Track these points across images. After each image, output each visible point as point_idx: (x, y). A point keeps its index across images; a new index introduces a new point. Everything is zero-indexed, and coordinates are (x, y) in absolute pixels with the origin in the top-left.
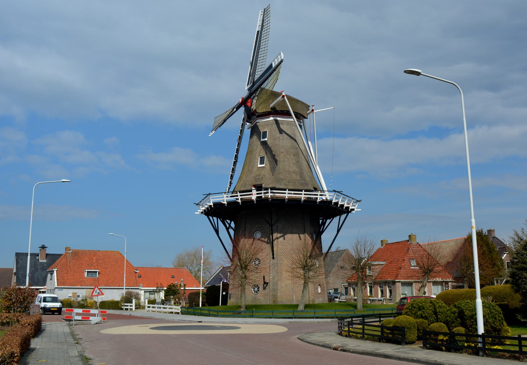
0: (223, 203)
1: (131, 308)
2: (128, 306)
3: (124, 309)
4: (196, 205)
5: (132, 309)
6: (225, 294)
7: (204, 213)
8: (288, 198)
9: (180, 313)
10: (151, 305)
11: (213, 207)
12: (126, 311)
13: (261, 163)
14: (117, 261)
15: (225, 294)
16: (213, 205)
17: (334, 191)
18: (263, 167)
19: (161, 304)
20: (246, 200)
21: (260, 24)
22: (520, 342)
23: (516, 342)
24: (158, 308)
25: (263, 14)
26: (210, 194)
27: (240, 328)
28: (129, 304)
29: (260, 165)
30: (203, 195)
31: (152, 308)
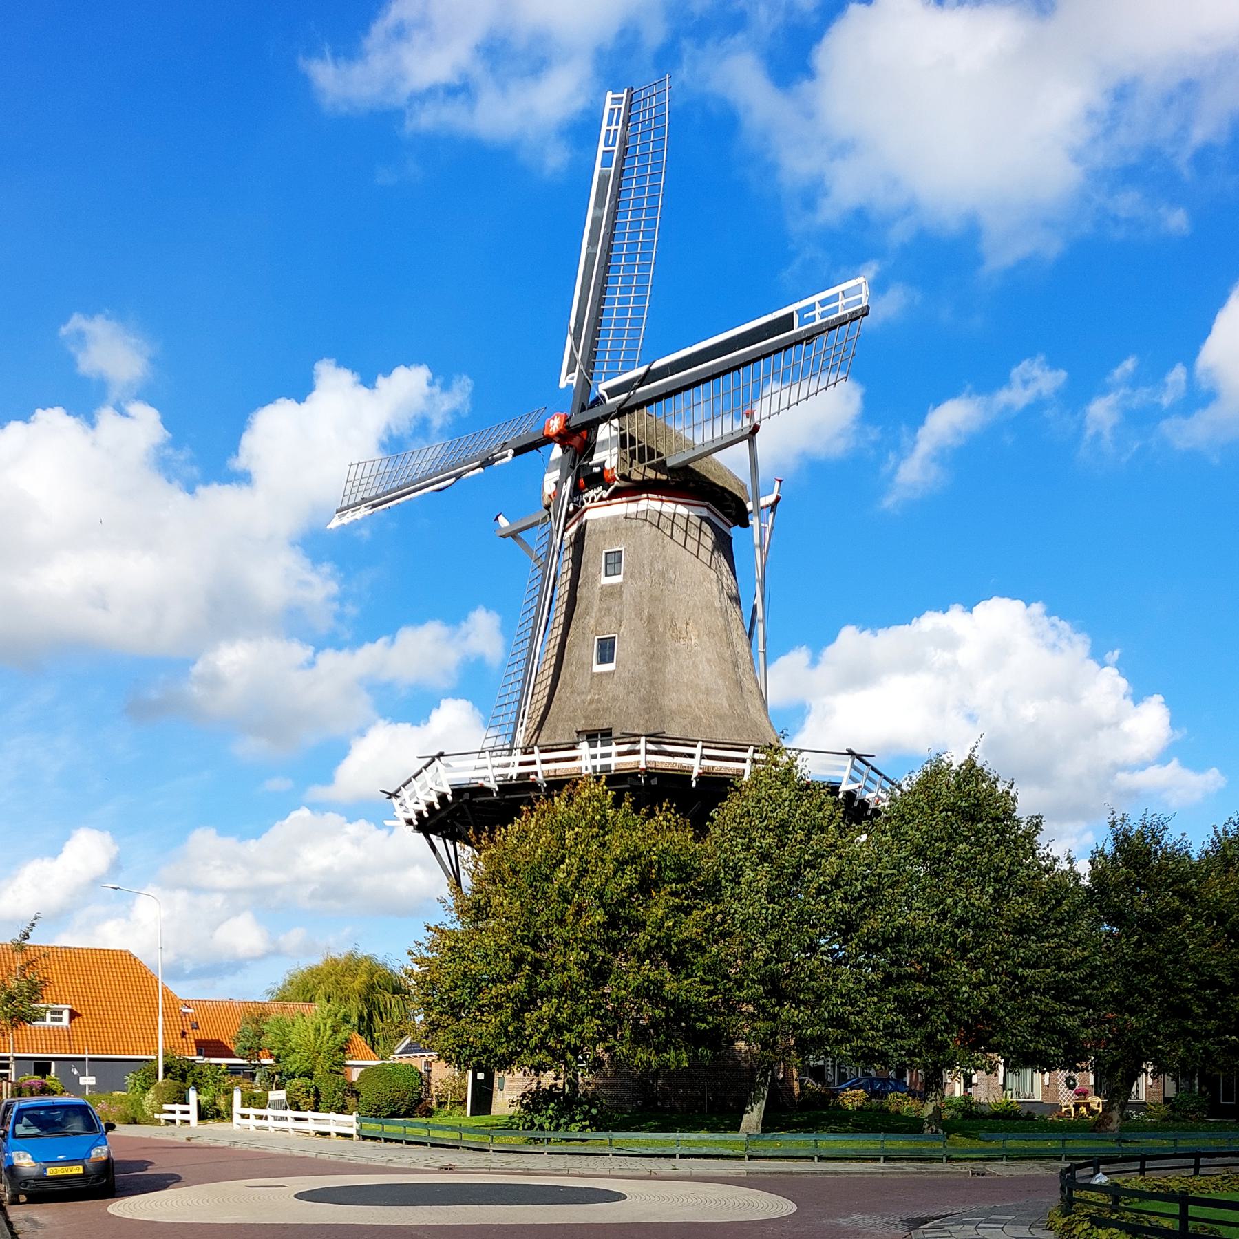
0: (486, 784)
1: (185, 1117)
2: (173, 1112)
3: (163, 1121)
4: (388, 796)
5: (188, 1122)
6: (483, 1078)
7: (416, 823)
8: (704, 773)
9: (356, 1137)
10: (251, 1111)
11: (450, 798)
12: (166, 1127)
13: (602, 660)
14: (566, 815)
15: (483, 1078)
16: (450, 792)
17: (851, 753)
18: (609, 674)
19: (286, 1108)
20: (555, 776)
21: (613, 144)
22: (1184, 1210)
23: (1175, 1209)
24: (275, 1118)
25: (624, 96)
26: (441, 754)
27: (619, 1197)
28: (177, 1107)
29: (598, 663)
30: (419, 758)
31: (275, 1120)
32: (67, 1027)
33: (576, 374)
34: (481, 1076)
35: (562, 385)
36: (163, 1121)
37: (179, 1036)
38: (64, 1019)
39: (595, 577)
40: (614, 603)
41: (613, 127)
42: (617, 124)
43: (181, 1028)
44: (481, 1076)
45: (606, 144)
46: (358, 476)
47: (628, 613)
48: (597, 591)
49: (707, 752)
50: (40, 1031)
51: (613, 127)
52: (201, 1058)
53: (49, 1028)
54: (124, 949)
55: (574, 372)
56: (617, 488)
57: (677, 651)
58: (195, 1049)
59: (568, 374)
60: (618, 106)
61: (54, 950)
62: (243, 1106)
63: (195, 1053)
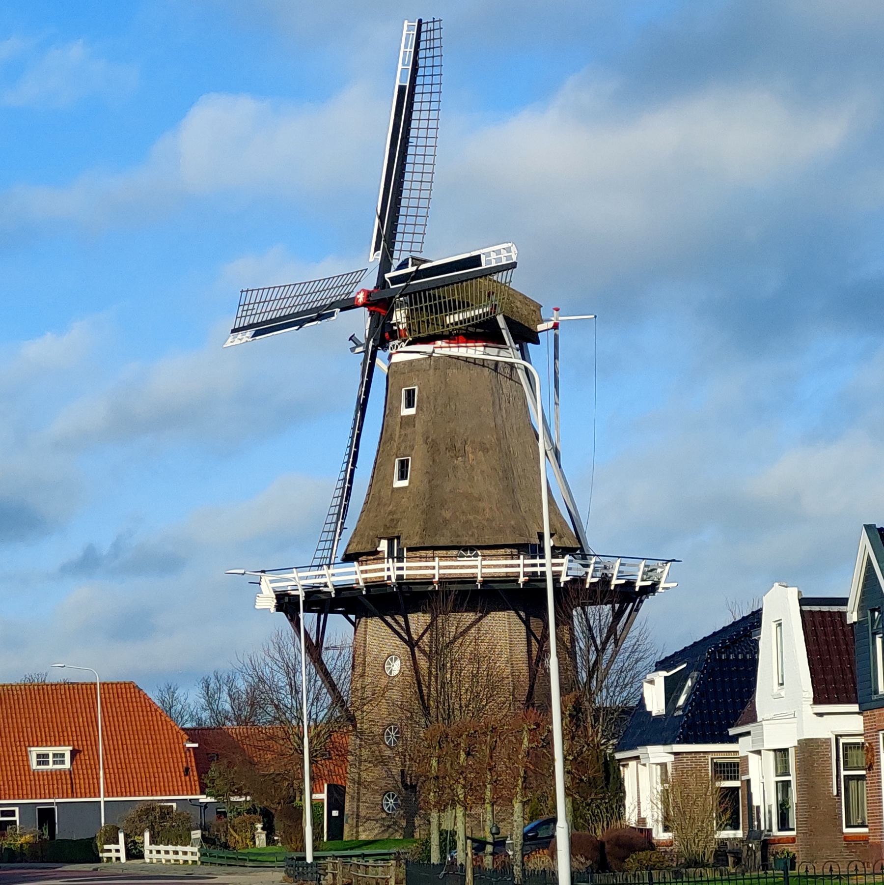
3: (105, 859)
32: (69, 769)
33: (380, 252)
34: (335, 813)
35: (371, 260)
36: (105, 859)
37: (182, 774)
38: (66, 762)
39: (399, 410)
40: (409, 431)
41: (408, 50)
42: (411, 48)
43: (185, 764)
44: (335, 813)
45: (403, 64)
46: (253, 301)
47: (419, 440)
48: (399, 420)
49: (442, 564)
50: (43, 776)
51: (408, 50)
52: (204, 796)
53: (51, 772)
54: (127, 681)
55: (379, 250)
56: (410, 341)
57: (455, 468)
58: (198, 788)
59: (375, 251)
60: (412, 32)
61: (58, 687)
62: (151, 844)
63: (198, 792)
